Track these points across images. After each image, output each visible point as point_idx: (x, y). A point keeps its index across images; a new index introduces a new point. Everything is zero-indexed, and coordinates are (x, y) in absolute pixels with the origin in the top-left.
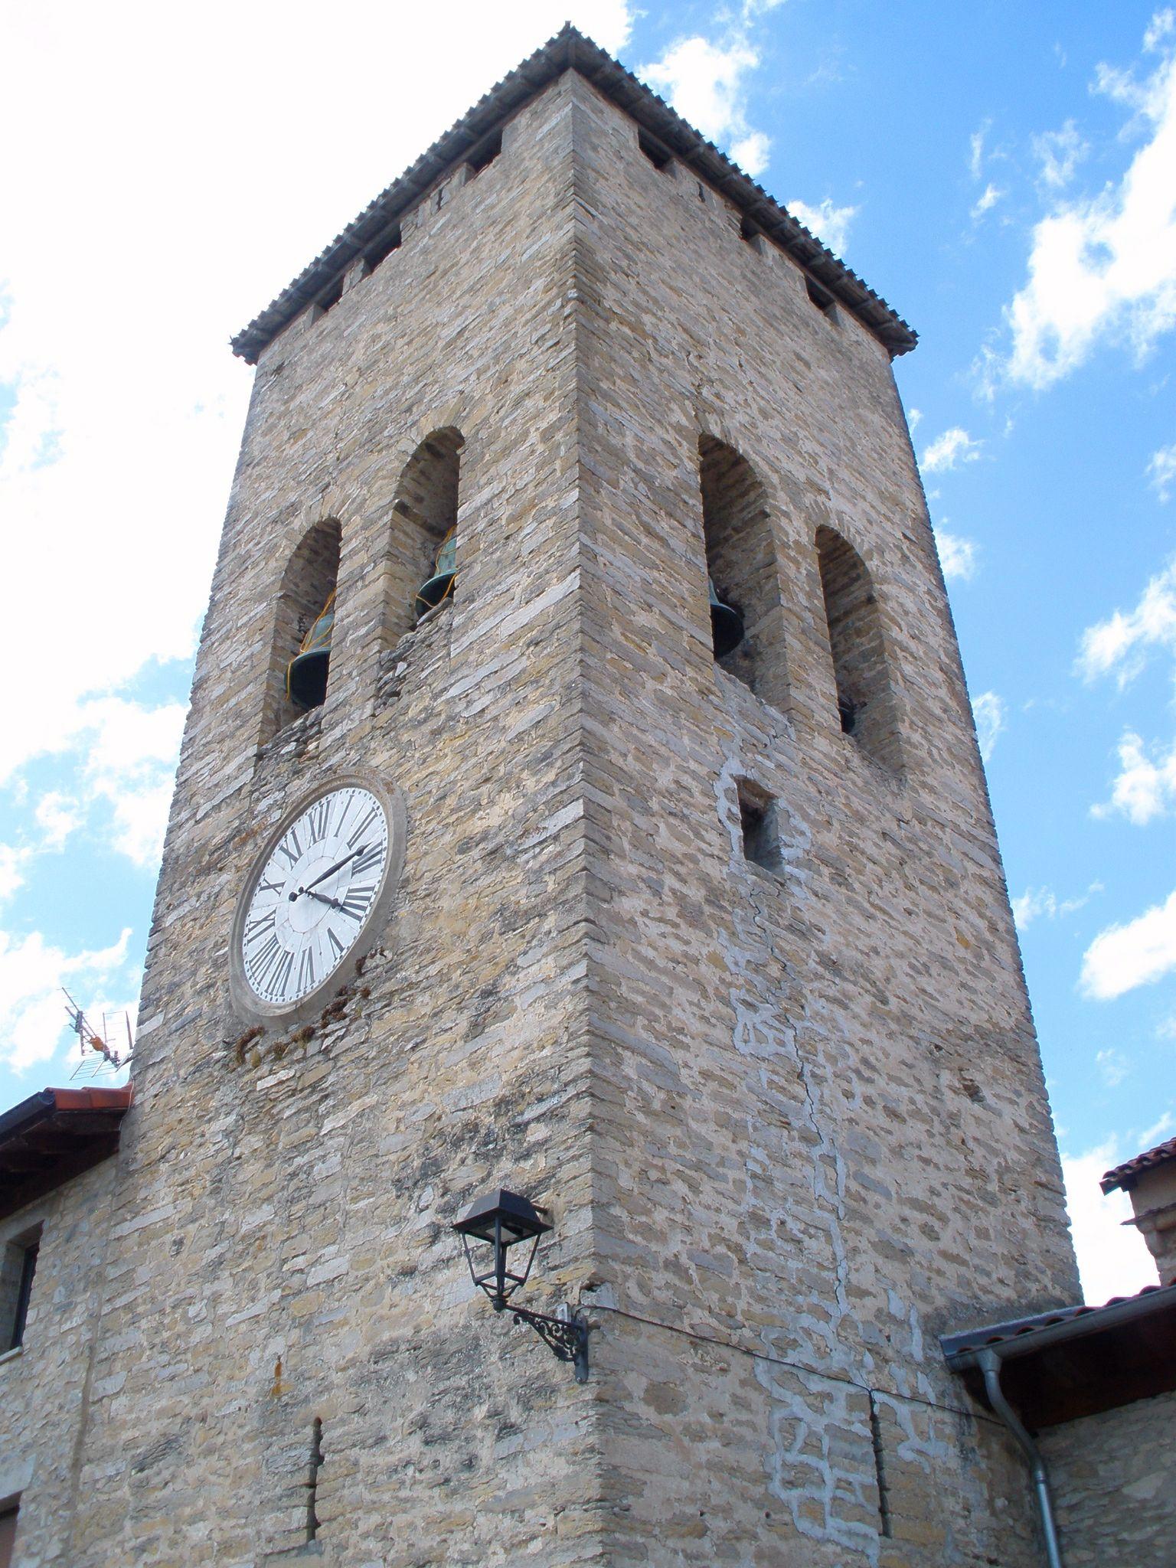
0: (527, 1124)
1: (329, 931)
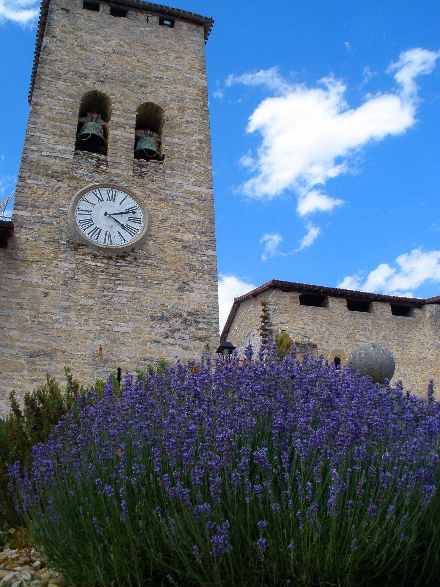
0: (200, 322)
1: (118, 232)
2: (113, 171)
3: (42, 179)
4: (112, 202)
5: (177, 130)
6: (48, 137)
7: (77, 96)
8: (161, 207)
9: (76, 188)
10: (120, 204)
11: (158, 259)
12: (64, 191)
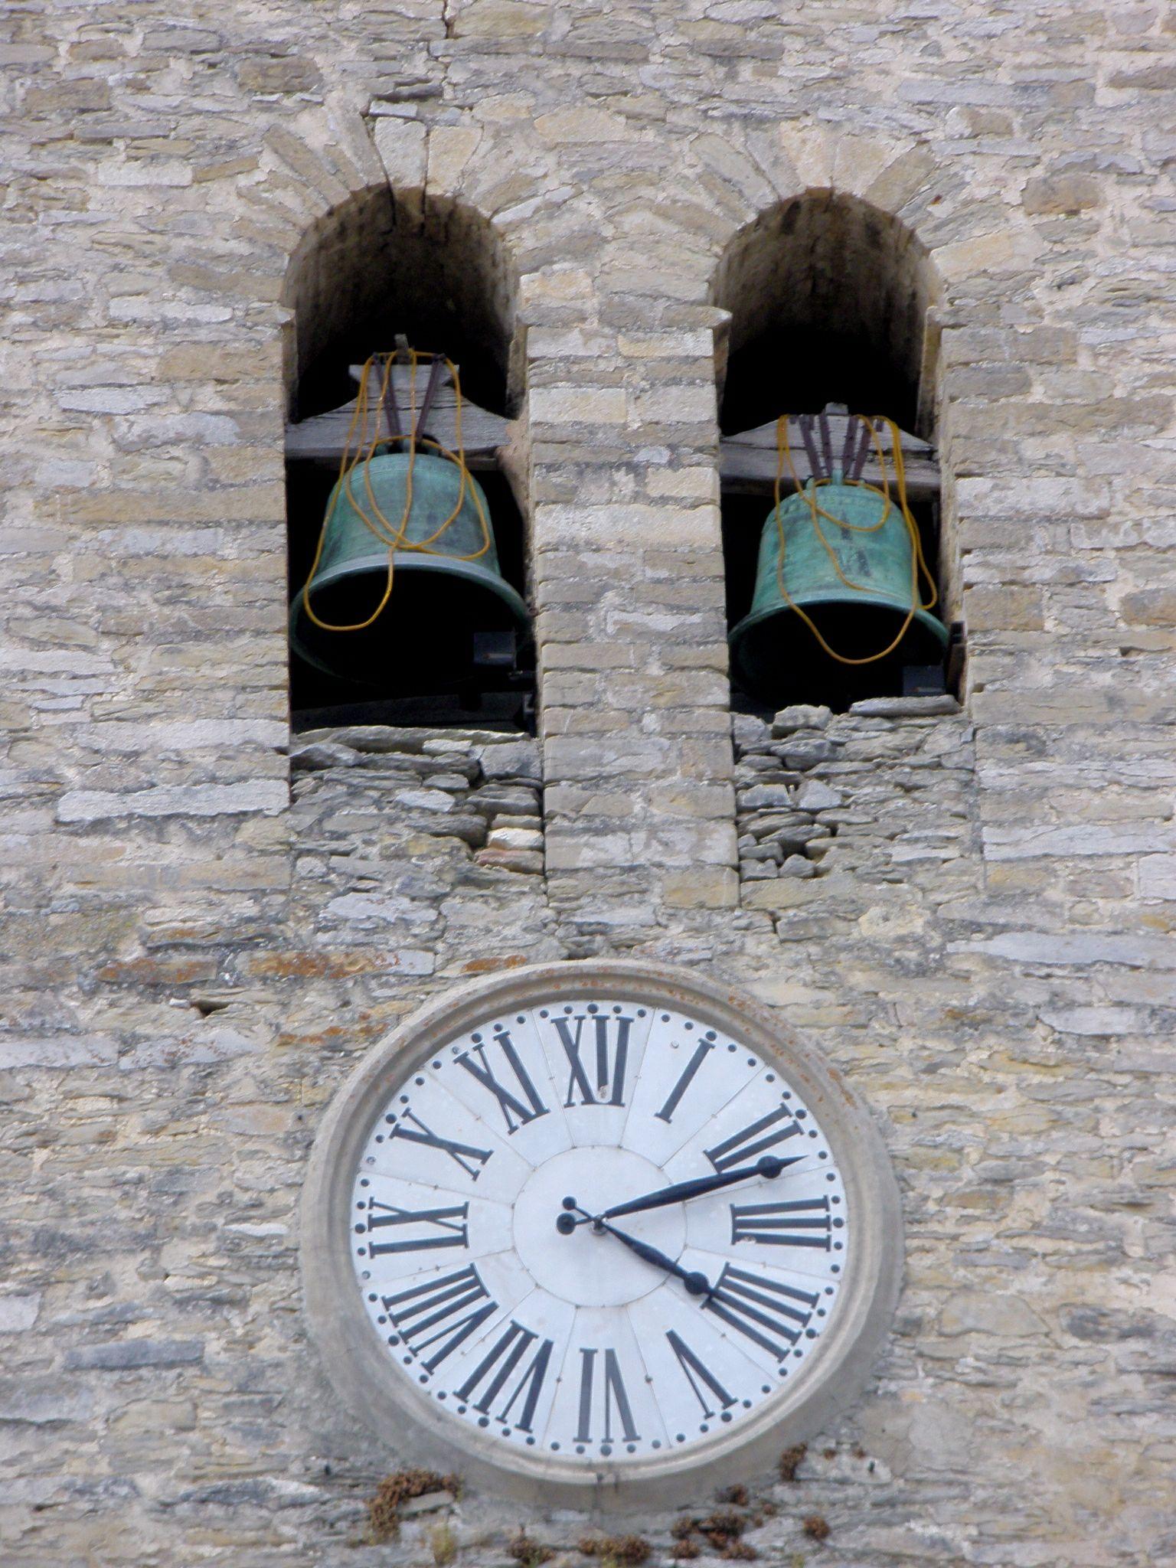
1: (672, 1337)
2: (588, 852)
3: (85, 1016)
4: (604, 1114)
5: (1037, 394)
6: (81, 663)
7: (248, 263)
8: (973, 1085)
9: (334, 1044)
10: (665, 1115)
11: (981, 1507)
12: (248, 1090)
